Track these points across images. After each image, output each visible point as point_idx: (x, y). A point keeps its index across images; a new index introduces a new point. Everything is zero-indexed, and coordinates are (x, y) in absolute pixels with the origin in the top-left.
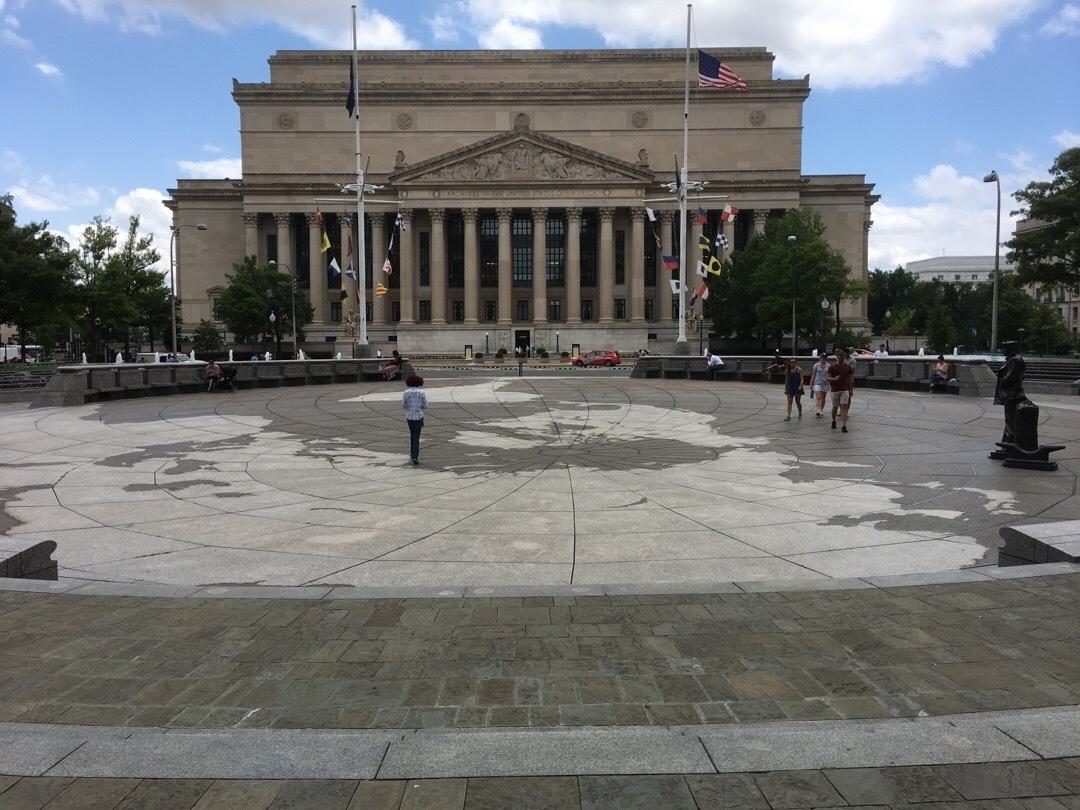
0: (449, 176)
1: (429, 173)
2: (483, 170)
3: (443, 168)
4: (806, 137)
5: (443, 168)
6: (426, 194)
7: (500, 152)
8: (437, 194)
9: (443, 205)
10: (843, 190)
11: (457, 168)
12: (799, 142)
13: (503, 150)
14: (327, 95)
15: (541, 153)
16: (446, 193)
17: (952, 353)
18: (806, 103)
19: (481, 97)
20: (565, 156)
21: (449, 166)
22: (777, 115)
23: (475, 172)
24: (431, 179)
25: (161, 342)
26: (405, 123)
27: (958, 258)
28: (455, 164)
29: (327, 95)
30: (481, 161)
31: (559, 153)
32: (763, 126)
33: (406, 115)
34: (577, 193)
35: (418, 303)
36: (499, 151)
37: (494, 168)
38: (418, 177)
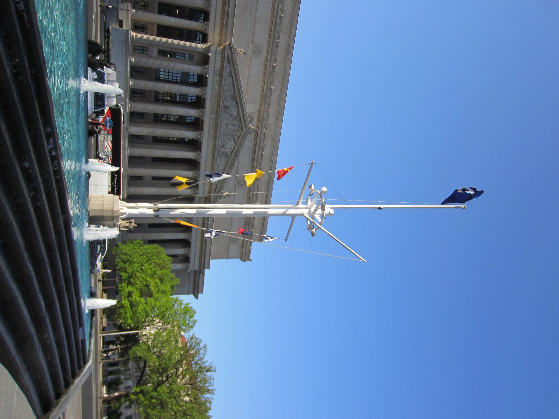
0: (227, 81)
1: (231, 70)
2: (228, 104)
3: (233, 80)
4: (224, 261)
5: (233, 80)
6: (218, 65)
7: (237, 116)
8: (217, 73)
9: (210, 76)
10: (197, 285)
11: (232, 88)
12: (221, 258)
13: (239, 118)
14: (278, 5)
15: (234, 139)
16: (218, 79)
17: (104, 267)
18: (239, 260)
19: (265, 98)
20: (231, 154)
21: (233, 84)
22: (235, 248)
23: (227, 99)
24: (227, 71)
25: (105, 316)
26: (257, 52)
27: (139, 148)
28: (234, 88)
29: (278, 5)
30: (234, 103)
31: (233, 151)
32: (230, 242)
33: (260, 51)
34: (210, 159)
35: (146, 46)
36: (238, 115)
37: (228, 111)
38: (229, 63)
